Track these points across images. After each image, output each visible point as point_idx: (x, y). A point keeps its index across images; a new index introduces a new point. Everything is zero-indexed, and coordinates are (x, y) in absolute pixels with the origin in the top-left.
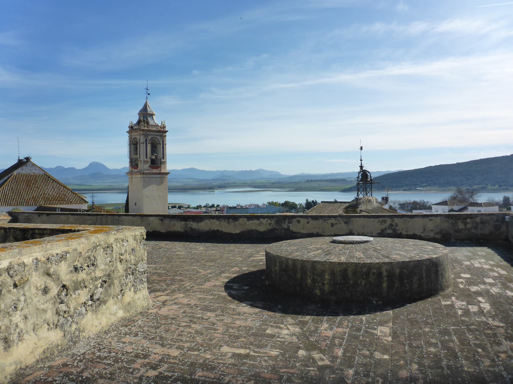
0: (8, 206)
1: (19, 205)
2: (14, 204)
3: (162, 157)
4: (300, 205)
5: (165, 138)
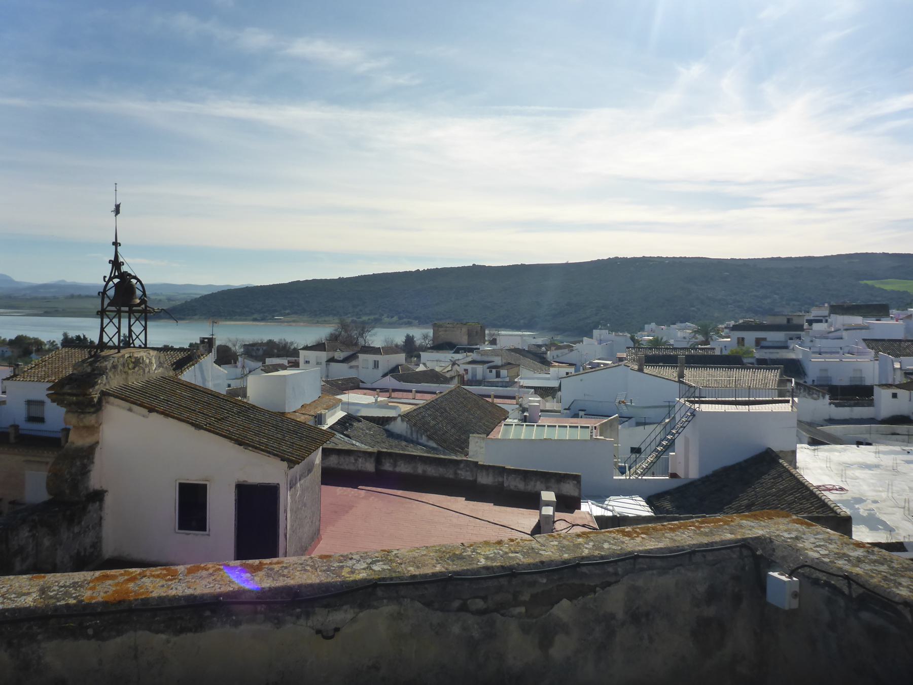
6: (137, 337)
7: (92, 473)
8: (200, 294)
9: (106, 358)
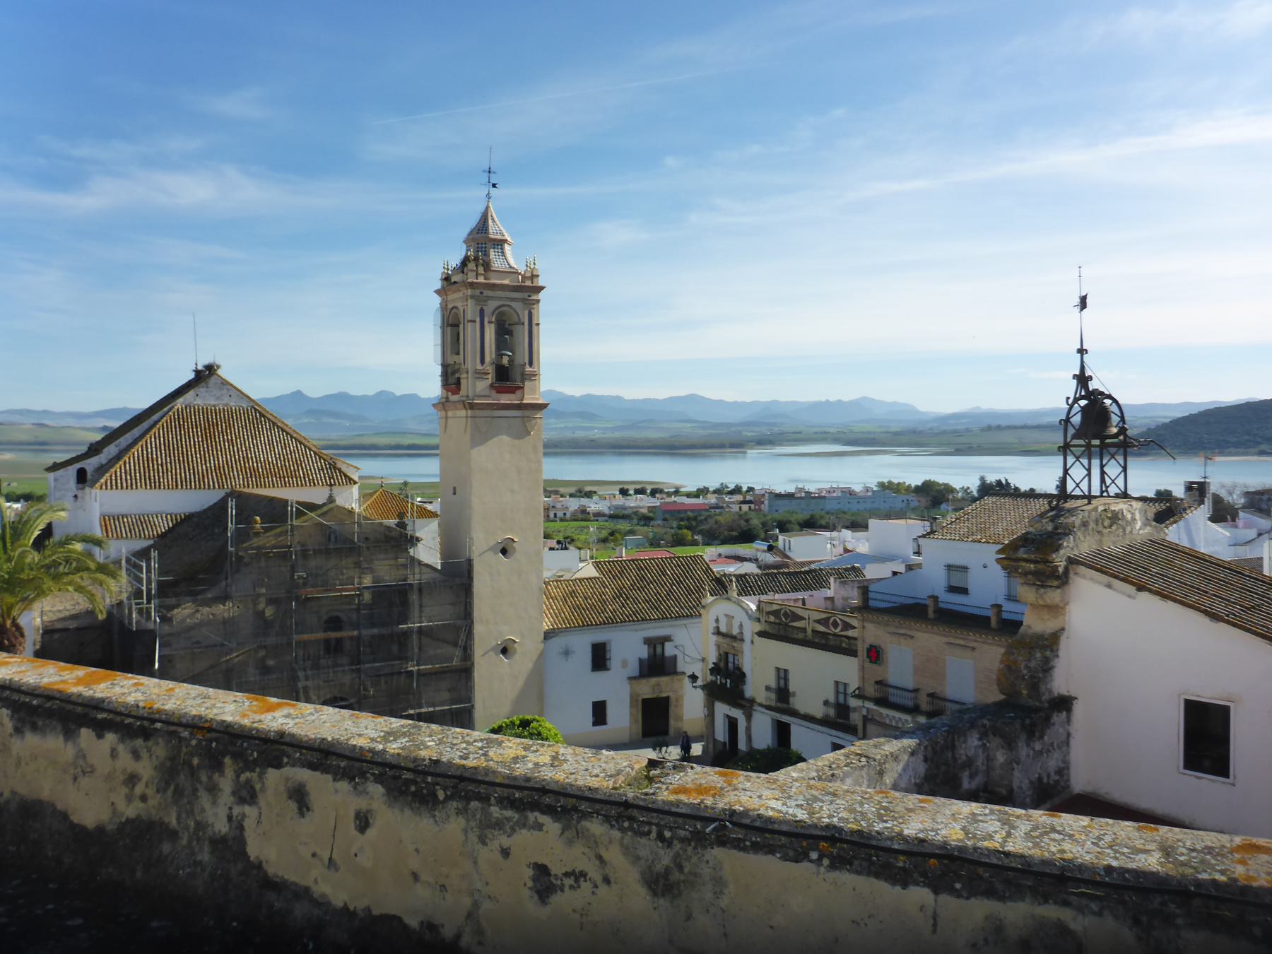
0: (151, 488)
1: (180, 487)
2: (168, 486)
3: (527, 361)
4: (966, 490)
5: (535, 306)
6: (1113, 481)
7: (1055, 669)
8: (1169, 417)
9: (1072, 511)
